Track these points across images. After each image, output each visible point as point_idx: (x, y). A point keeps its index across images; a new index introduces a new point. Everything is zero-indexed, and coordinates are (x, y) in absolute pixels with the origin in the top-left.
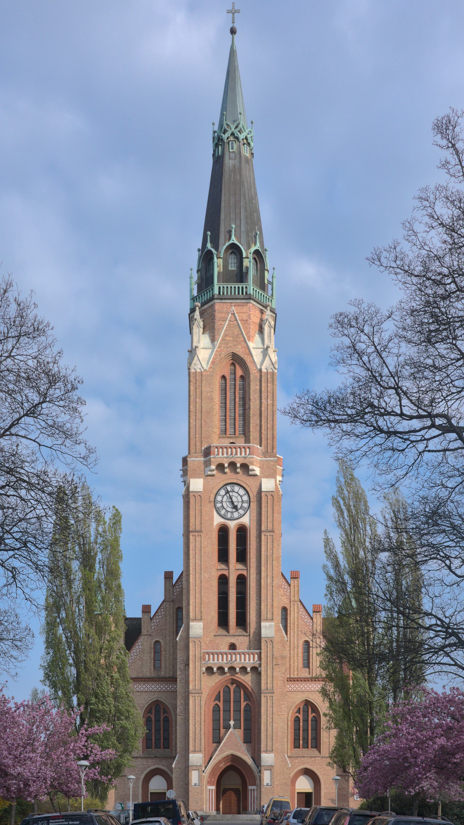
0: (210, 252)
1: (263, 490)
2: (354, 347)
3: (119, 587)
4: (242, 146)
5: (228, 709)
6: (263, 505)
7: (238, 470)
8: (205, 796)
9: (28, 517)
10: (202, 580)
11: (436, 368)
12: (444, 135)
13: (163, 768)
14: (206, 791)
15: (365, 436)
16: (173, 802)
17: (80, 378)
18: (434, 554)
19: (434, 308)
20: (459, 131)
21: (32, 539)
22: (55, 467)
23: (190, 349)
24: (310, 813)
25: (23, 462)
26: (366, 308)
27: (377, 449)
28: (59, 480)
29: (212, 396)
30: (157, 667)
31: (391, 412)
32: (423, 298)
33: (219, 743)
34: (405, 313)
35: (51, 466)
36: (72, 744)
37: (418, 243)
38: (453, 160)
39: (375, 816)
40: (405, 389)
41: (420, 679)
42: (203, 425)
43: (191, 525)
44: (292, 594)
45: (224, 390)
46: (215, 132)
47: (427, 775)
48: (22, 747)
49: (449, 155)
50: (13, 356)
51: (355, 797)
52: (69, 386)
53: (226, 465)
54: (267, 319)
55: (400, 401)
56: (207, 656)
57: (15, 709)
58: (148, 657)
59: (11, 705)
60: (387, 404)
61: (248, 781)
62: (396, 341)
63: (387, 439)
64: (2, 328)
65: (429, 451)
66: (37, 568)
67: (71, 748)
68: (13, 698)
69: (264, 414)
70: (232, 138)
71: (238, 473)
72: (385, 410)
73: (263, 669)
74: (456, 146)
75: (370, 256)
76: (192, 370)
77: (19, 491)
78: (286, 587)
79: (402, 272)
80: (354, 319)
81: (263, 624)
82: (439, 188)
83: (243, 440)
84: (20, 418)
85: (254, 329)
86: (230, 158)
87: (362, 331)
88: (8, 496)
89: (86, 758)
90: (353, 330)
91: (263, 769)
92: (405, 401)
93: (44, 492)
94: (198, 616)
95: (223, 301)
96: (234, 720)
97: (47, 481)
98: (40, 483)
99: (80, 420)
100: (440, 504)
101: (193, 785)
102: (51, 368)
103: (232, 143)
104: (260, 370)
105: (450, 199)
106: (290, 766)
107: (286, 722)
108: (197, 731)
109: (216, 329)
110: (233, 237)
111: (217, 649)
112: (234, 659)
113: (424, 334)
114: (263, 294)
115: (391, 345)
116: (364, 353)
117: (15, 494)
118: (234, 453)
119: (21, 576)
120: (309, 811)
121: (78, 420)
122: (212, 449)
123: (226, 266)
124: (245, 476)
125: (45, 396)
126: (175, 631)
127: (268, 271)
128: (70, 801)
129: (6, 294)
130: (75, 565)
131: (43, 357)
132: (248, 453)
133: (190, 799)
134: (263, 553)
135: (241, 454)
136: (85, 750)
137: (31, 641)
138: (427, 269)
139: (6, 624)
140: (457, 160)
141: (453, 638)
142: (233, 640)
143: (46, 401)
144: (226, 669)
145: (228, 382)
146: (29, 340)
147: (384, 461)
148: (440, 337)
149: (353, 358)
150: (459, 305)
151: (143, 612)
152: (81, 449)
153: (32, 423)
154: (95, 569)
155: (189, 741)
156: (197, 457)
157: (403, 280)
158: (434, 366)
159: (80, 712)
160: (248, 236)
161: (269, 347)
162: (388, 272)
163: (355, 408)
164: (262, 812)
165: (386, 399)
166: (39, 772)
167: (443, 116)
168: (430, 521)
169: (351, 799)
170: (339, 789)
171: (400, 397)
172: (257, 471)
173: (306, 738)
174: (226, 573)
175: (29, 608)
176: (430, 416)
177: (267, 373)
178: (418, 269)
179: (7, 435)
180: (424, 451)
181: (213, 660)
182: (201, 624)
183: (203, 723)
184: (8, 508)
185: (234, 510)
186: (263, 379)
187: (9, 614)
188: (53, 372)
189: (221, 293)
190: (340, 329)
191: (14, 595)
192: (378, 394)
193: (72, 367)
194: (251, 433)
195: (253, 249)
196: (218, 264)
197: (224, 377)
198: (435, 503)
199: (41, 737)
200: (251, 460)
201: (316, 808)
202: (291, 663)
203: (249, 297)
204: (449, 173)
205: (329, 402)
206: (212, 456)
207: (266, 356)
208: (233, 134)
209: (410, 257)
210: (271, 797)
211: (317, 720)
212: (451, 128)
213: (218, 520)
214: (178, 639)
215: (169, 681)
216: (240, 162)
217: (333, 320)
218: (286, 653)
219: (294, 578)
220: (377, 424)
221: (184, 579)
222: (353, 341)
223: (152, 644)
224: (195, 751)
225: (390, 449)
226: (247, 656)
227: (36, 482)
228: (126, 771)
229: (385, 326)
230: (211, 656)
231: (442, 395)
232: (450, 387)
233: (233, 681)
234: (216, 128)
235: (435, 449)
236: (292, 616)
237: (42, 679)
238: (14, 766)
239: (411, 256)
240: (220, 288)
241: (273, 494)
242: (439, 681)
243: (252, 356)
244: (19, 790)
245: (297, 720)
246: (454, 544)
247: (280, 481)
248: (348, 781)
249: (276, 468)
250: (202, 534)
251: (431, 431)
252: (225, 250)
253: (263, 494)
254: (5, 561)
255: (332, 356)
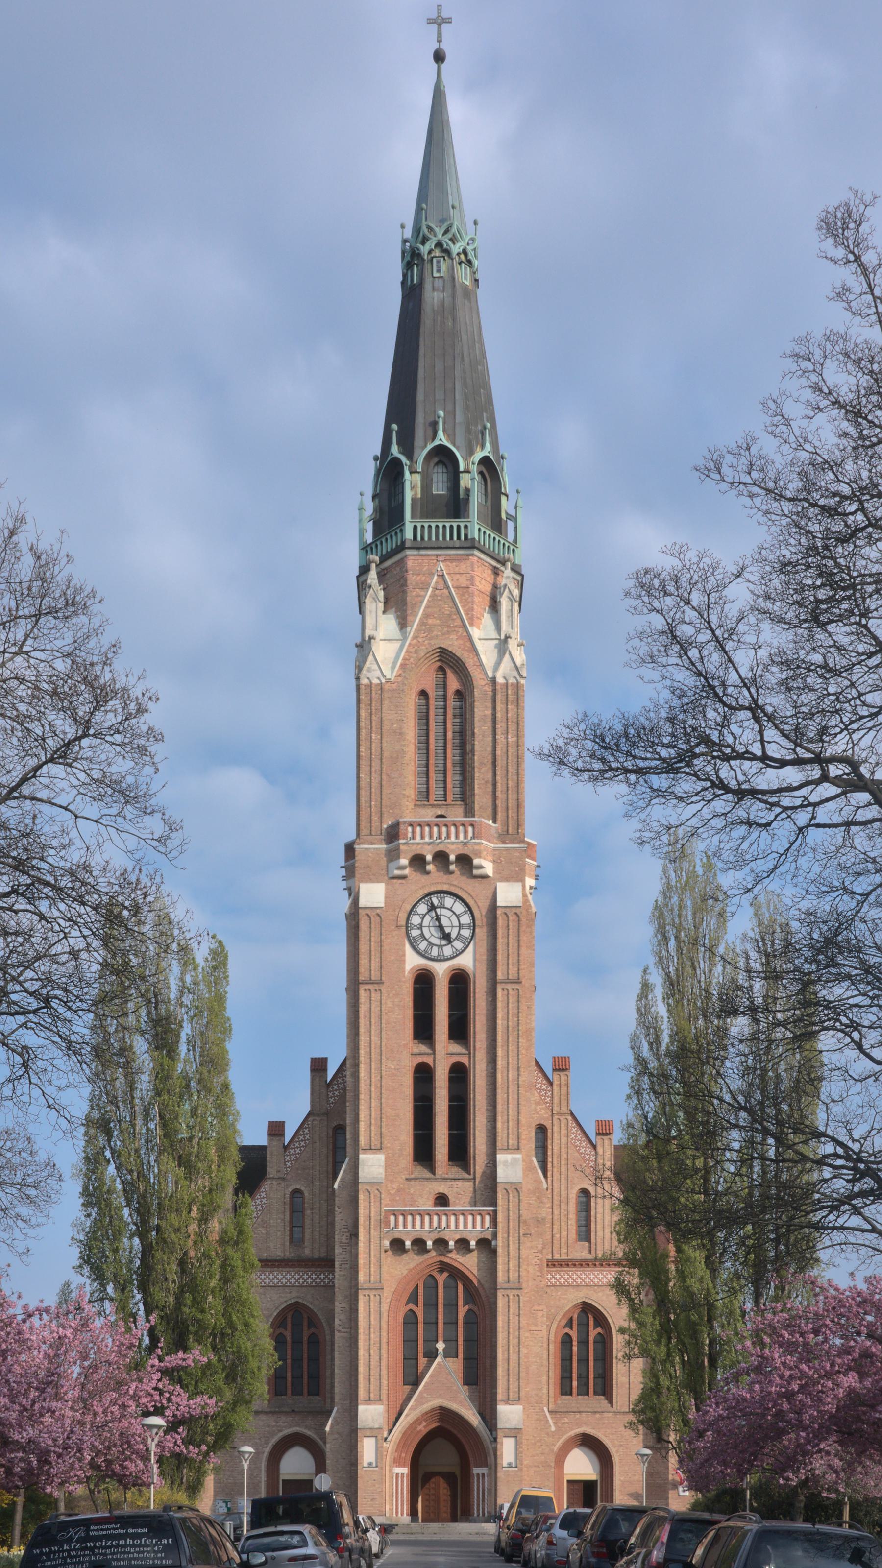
0: (397, 463)
1: (499, 904)
2: (672, 632)
3: (226, 1087)
4: (456, 266)
5: (434, 1320)
6: (500, 932)
7: (452, 867)
8: (389, 1486)
9: (53, 952)
10: (384, 1073)
11: (830, 670)
12: (839, 239)
13: (308, 1433)
14: (391, 1477)
15: (694, 799)
16: (326, 1496)
17: (153, 691)
18: (829, 1020)
19: (824, 558)
20: (868, 231)
21: (59, 993)
22: (106, 857)
23: (358, 640)
24: (593, 1518)
25: (44, 848)
26: (695, 560)
27: (718, 823)
28: (112, 880)
29: (401, 728)
30: (295, 1241)
31: (744, 753)
32: (803, 540)
33: (416, 1383)
34: (768, 568)
35: (97, 855)
36: (133, 1386)
37: (792, 439)
38: (857, 285)
39: (719, 1522)
40: (769, 710)
41: (805, 1258)
42: (384, 783)
43: (362, 970)
44: (556, 1101)
45: (424, 718)
46: (405, 241)
47: (822, 1446)
48: (37, 1389)
49: (848, 275)
50: (27, 653)
51: (681, 1489)
52: (133, 707)
53: (429, 858)
54: (505, 586)
55: (761, 732)
56: (392, 1218)
57: (23, 1316)
58: (279, 1221)
59: (17, 1311)
60: (735, 738)
61: (471, 1459)
62: (752, 619)
63: (736, 804)
64: (8, 601)
65: (818, 826)
66: (70, 1048)
67: (131, 1392)
68: (19, 1297)
69: (500, 762)
70: (437, 253)
71: (452, 873)
72: (733, 750)
73: (500, 1244)
74: (863, 259)
75: (701, 463)
76: (364, 681)
77: (37, 903)
78: (544, 1087)
79: (763, 492)
80: (671, 579)
81: (500, 1157)
82: (832, 337)
83: (460, 810)
84: (40, 766)
85: (481, 603)
86: (434, 289)
87: (688, 603)
88: (16, 912)
89: (159, 1411)
90: (669, 601)
91: (500, 1434)
92: (771, 733)
93: (83, 904)
94: (375, 1143)
95: (423, 552)
96: (444, 1341)
97: (89, 883)
98: (77, 885)
99: (152, 769)
100: (841, 924)
101: (366, 1465)
102: (98, 673)
103: (438, 262)
104: (494, 681)
105: (852, 356)
106: (553, 1429)
107: (545, 1345)
108: (374, 1362)
109: (409, 604)
110: (441, 434)
111: (412, 1206)
112: (444, 1224)
113: (806, 607)
114: (497, 539)
115: (742, 628)
116: (691, 644)
117: (29, 907)
118: (444, 835)
119: (39, 1063)
120: (592, 1513)
121: (149, 770)
122: (402, 827)
123: (428, 484)
124: (464, 878)
125: (87, 724)
126: (330, 1171)
127: (507, 496)
128: (129, 1495)
129: (15, 538)
130: (140, 1045)
131: (83, 654)
132: (470, 834)
133: (360, 1493)
134: (499, 1022)
135: (457, 837)
136: (157, 1398)
137: (55, 1187)
138: (809, 486)
139: (9, 1155)
140: (865, 285)
141: (867, 1179)
142: (442, 1188)
143: (89, 735)
144: (430, 1244)
145: (432, 702)
146: (57, 621)
147: (731, 844)
148: (837, 611)
149: (670, 652)
150: (873, 552)
151: (269, 1135)
152: (154, 825)
153: (63, 775)
154: (179, 1054)
155: (357, 1380)
156: (373, 844)
157: (764, 507)
158: (825, 666)
159: (148, 1325)
160: (468, 431)
161: (510, 637)
162: (734, 492)
163: (674, 746)
164: (500, 1517)
165: (734, 728)
166: (68, 1438)
167: (836, 205)
168: (821, 957)
169: (672, 1494)
170: (650, 1475)
171: (761, 726)
172: (489, 868)
173: (584, 1375)
174: (428, 1060)
175: (54, 1123)
176: (819, 760)
177: (506, 685)
178: (794, 486)
179: (15, 798)
180: (807, 826)
181: (405, 1226)
182: (380, 1158)
183: (384, 1346)
184: (16, 934)
185: (444, 942)
186: (499, 697)
187: (14, 1135)
188: (102, 681)
189: (419, 538)
190: (646, 599)
191: (25, 1098)
192: (719, 719)
193: (137, 672)
194: (476, 797)
195: (478, 455)
196: (412, 485)
197: (423, 694)
198: (830, 924)
199: (72, 1372)
200: (476, 847)
201: (605, 1507)
202: (555, 1231)
203: (471, 545)
204: (849, 308)
205: (626, 735)
206: (401, 841)
207: (504, 653)
208: (439, 245)
209: (777, 465)
210: (516, 1489)
211: (605, 1342)
212: (852, 225)
213: (413, 961)
214: (336, 1186)
215: (318, 1266)
216: (453, 296)
217: (632, 583)
218: (545, 1212)
219: (560, 1070)
220: (718, 777)
221: (348, 1073)
222: (670, 621)
223: (288, 1196)
224: (369, 1401)
225: (742, 822)
226: (470, 1218)
227: (70, 885)
228: (237, 1436)
229: (731, 592)
230: (401, 1218)
231: (842, 721)
232: (856, 706)
233: (444, 1267)
234: (408, 234)
235: (829, 822)
236: (556, 1141)
237: (77, 1263)
238: (20, 1426)
239: (780, 462)
240: (415, 528)
241: (518, 911)
242: (842, 1265)
243: (478, 655)
244: (29, 1470)
245: (566, 1341)
246: (868, 1002)
247: (531, 888)
248: (666, 1457)
249: (525, 864)
250: (383, 988)
251: (820, 788)
252: (425, 458)
253: (499, 912)
254: (9, 1035)
255: (630, 650)
